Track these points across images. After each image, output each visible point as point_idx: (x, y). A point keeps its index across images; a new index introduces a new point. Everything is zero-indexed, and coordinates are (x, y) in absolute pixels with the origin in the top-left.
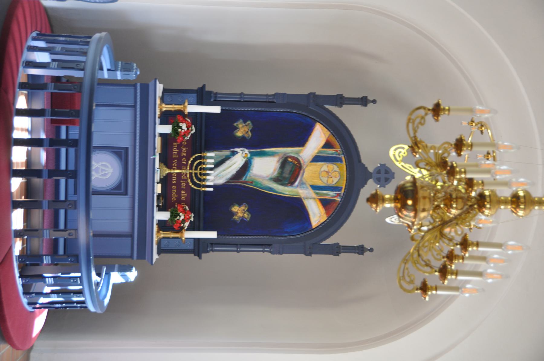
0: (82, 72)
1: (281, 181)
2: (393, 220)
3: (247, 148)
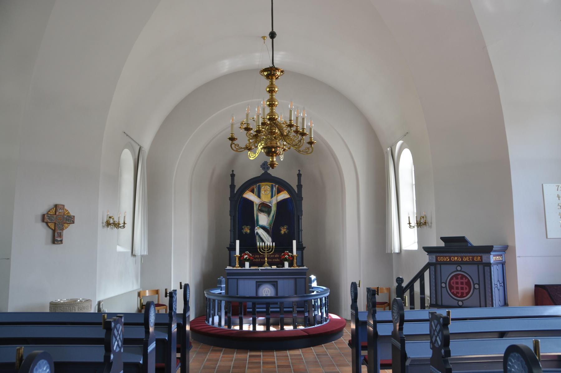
0: (222, 301)
1: (269, 212)
2: (282, 157)
3: (255, 228)
